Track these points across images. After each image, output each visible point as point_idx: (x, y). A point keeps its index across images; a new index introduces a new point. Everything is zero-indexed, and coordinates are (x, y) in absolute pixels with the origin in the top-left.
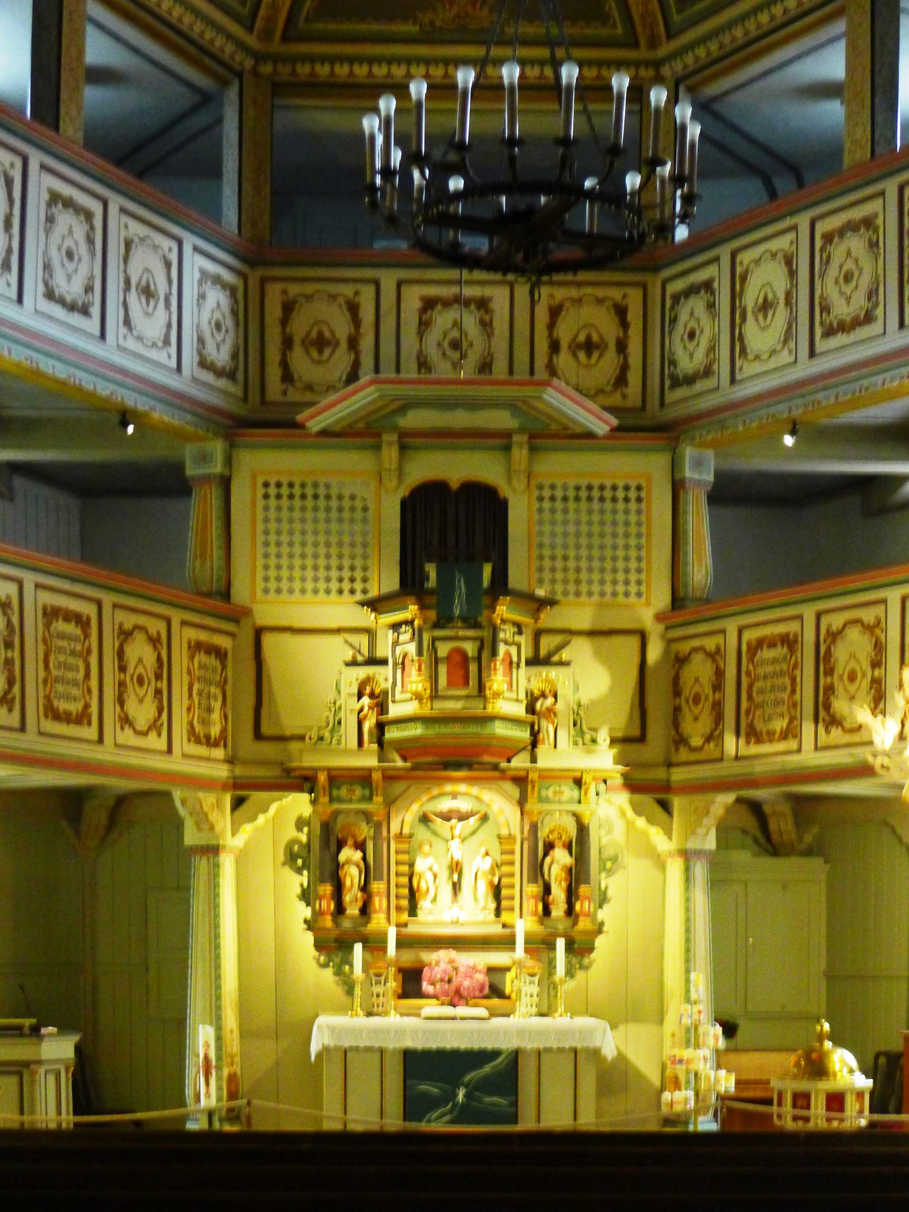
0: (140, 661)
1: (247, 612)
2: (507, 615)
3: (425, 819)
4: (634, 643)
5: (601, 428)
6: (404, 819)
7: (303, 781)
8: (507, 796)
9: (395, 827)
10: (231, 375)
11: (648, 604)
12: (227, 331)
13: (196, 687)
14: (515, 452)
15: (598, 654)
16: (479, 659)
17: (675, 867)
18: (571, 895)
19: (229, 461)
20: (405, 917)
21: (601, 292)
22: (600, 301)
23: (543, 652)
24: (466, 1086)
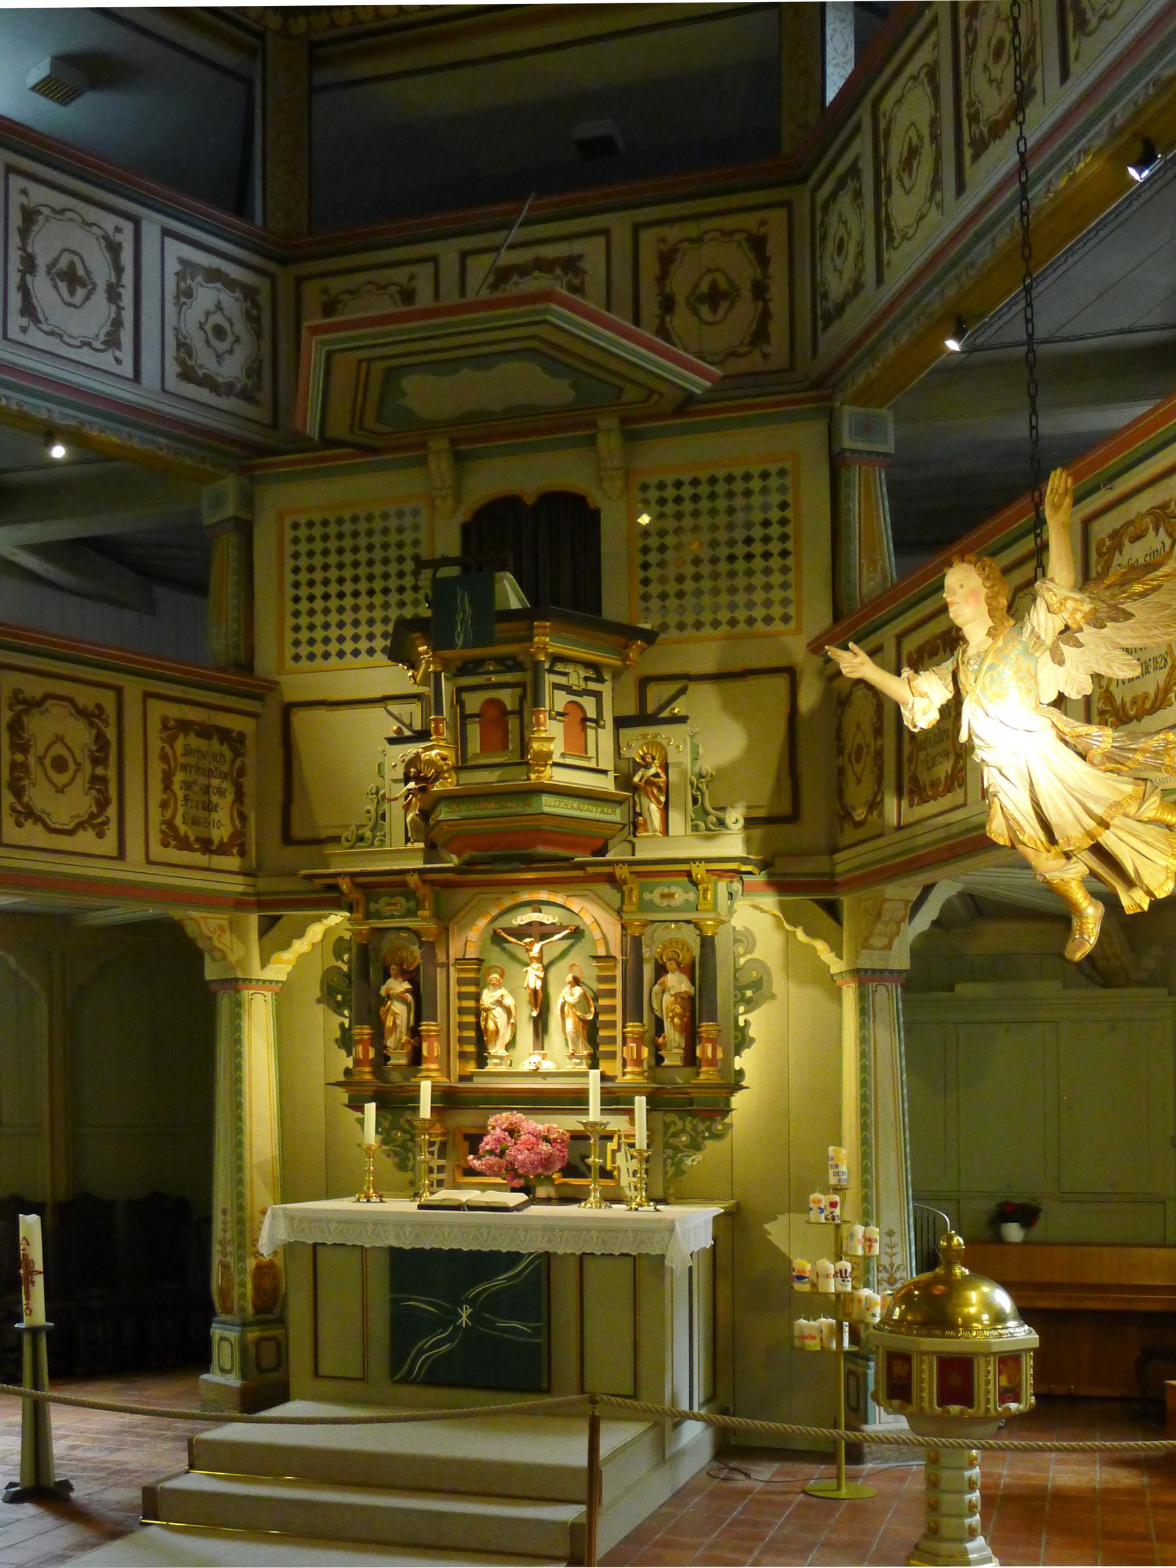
0: (59, 739)
1: (272, 686)
2: (555, 648)
3: (497, 939)
4: (780, 683)
5: (698, 385)
6: (470, 939)
7: (328, 896)
8: (607, 905)
9: (455, 950)
10: (247, 395)
11: (799, 630)
12: (237, 340)
13: (179, 778)
14: (602, 441)
15: (730, 706)
16: (520, 713)
17: (849, 994)
18: (692, 1037)
19: (248, 501)
20: (471, 1067)
21: (729, 223)
22: (728, 234)
23: (650, 709)
24: (471, 1302)
